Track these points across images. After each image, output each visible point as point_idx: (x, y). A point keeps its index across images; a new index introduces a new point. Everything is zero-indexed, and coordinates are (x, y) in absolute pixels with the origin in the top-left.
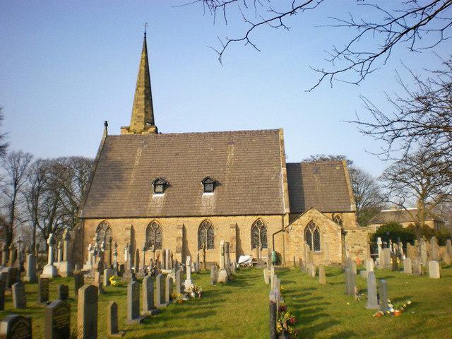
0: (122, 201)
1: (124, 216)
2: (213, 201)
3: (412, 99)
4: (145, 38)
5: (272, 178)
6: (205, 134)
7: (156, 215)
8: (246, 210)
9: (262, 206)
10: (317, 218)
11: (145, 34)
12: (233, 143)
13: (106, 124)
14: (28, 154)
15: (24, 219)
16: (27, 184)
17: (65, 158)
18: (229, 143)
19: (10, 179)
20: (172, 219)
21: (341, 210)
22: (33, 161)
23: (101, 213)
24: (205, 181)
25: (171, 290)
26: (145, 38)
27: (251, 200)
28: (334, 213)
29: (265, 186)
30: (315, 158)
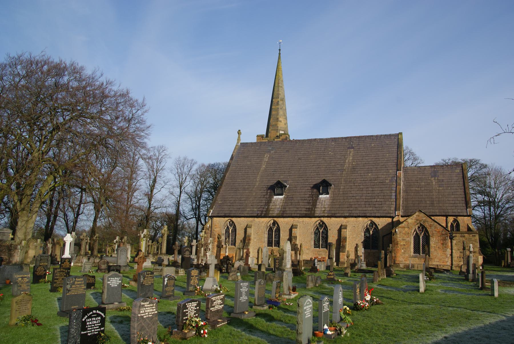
0: (246, 202)
1: (246, 215)
2: (327, 203)
3: (93, 76)
4: (280, 54)
5: (387, 181)
6: (327, 139)
7: (275, 215)
8: (358, 212)
9: (374, 209)
10: (424, 222)
11: (280, 50)
12: (353, 148)
13: (239, 133)
14: (192, 160)
15: (189, 217)
16: (189, 186)
17: (220, 164)
18: (349, 148)
19: (176, 183)
20: (289, 219)
21: (457, 214)
22: (195, 167)
23: (226, 212)
24: (316, 187)
25: (474, 272)
26: (280, 54)
27: (363, 203)
28: (447, 216)
29: (379, 189)
30: (447, 161)
